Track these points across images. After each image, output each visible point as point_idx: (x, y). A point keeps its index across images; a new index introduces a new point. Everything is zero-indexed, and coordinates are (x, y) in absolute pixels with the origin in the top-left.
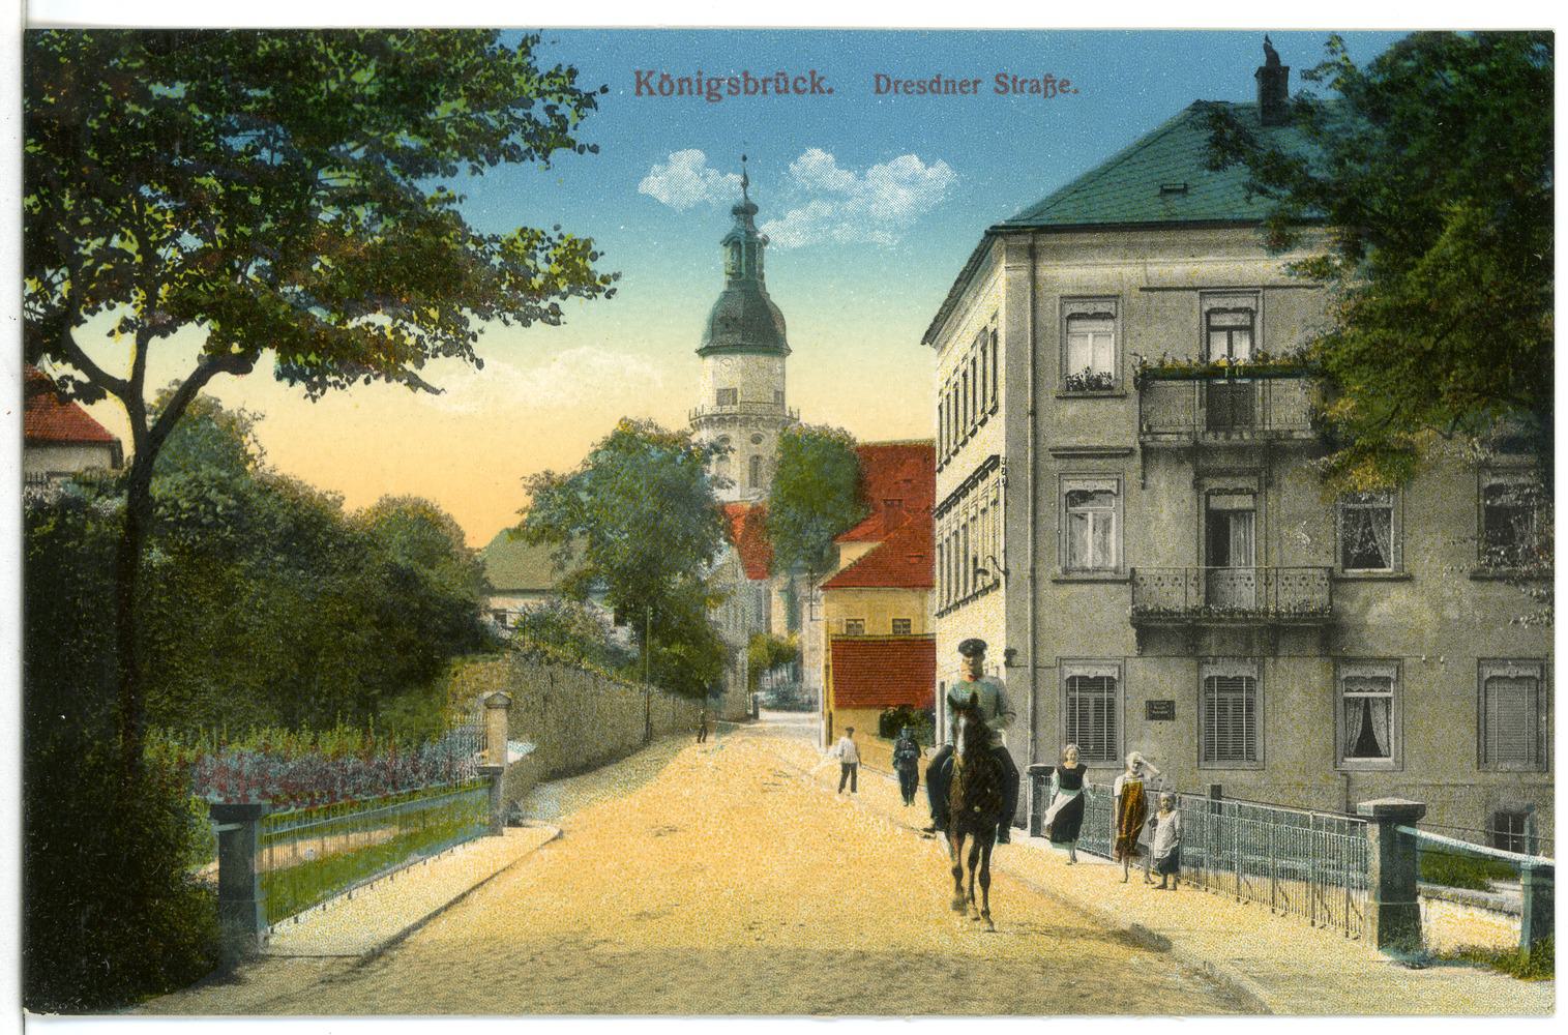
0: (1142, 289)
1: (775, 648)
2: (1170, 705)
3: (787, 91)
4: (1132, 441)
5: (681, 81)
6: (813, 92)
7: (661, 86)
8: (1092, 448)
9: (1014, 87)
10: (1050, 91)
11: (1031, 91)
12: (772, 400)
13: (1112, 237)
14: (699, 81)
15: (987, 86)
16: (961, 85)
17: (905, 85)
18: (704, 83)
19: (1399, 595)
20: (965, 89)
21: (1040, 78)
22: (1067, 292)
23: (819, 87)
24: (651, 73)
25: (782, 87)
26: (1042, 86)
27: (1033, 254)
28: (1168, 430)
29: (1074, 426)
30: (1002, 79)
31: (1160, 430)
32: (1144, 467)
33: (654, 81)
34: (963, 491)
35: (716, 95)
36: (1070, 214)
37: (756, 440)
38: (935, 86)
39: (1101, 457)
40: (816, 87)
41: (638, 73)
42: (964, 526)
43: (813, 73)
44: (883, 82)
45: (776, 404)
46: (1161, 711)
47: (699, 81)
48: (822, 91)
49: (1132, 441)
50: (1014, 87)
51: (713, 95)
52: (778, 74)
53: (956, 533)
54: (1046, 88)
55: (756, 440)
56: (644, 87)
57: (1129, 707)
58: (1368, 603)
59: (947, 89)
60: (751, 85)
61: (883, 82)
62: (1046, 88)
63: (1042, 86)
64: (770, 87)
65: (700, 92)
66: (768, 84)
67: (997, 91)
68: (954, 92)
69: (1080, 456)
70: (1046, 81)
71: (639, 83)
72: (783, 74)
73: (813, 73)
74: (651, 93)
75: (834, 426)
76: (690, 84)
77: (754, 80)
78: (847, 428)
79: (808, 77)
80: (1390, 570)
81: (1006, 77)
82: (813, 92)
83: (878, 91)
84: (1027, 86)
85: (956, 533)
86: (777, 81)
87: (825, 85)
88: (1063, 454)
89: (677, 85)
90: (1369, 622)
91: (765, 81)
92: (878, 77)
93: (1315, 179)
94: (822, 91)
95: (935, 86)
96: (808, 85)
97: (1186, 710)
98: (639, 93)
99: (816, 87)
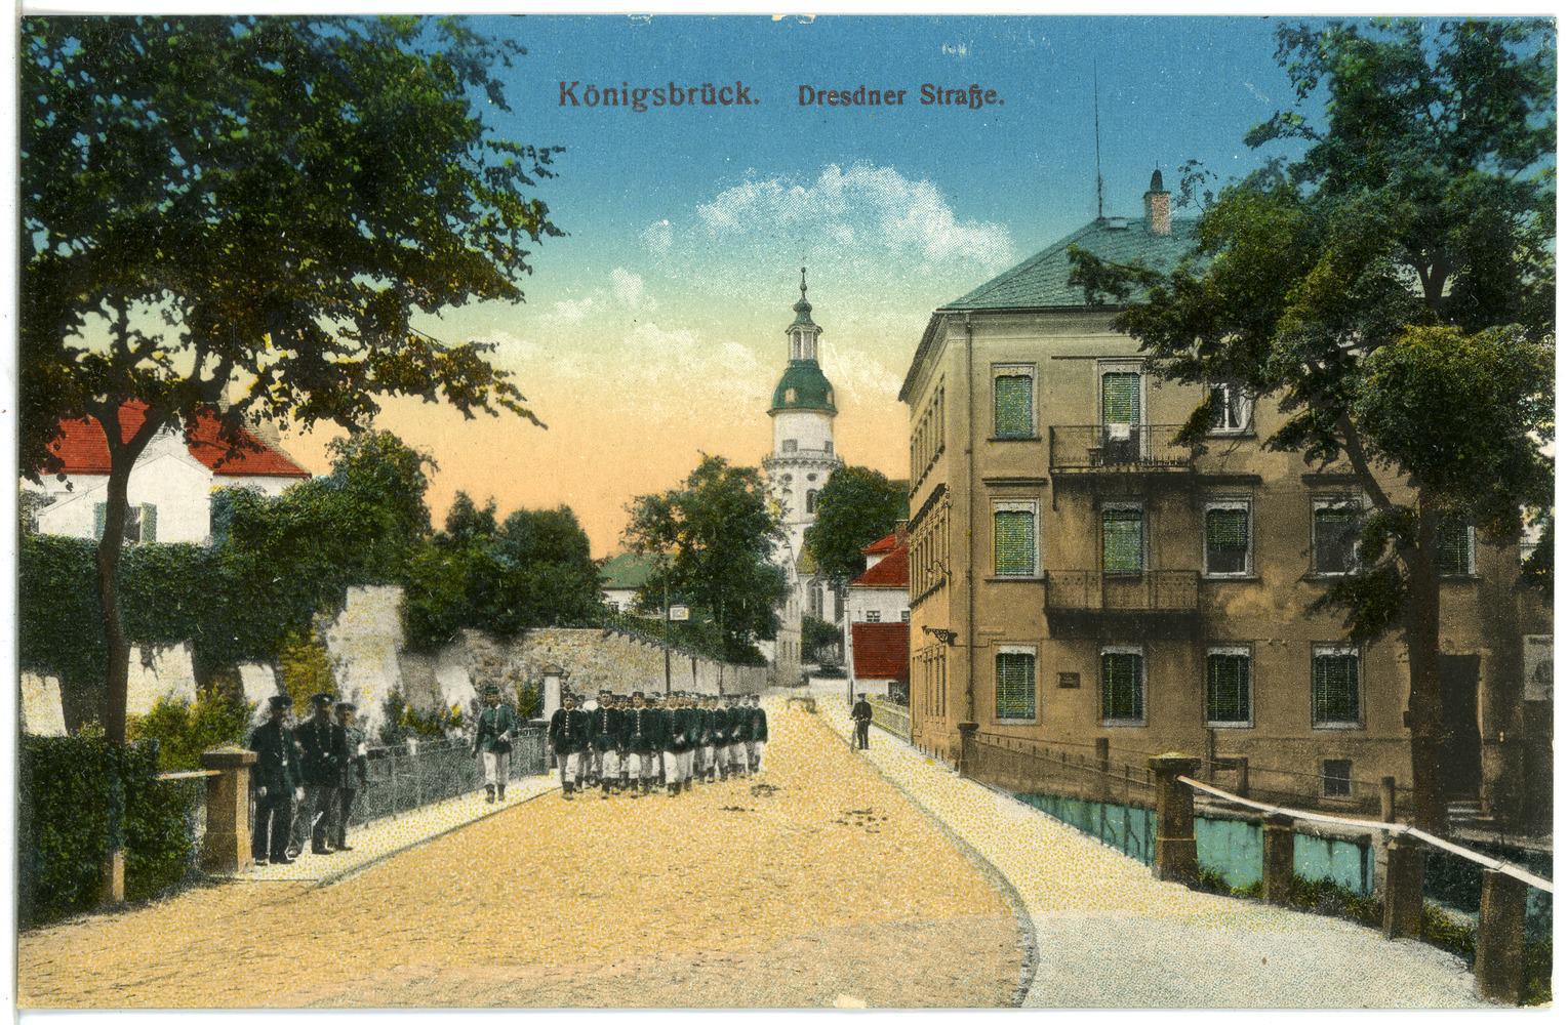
0: (1053, 358)
1: (1544, 62)
2: (1076, 676)
3: (713, 102)
4: (1044, 473)
5: (606, 92)
6: (739, 102)
7: (586, 95)
8: (1031, 479)
9: (940, 98)
10: (976, 103)
11: (958, 102)
12: (823, 448)
13: (1027, 319)
14: (625, 92)
15: (914, 94)
16: (887, 96)
17: (830, 96)
18: (630, 94)
19: (1251, 594)
20: (890, 100)
21: (967, 89)
22: (996, 359)
23: (746, 98)
24: (575, 84)
25: (708, 98)
26: (968, 96)
27: (970, 331)
28: (1073, 464)
29: (1000, 462)
30: (928, 89)
31: (1067, 464)
32: (1055, 494)
33: (579, 93)
34: (924, 512)
35: (642, 105)
36: (998, 300)
37: (812, 477)
38: (859, 97)
39: (1023, 485)
40: (742, 96)
41: (563, 85)
42: (931, 533)
43: (739, 84)
44: (807, 94)
45: (826, 452)
46: (1068, 681)
47: (625, 92)
48: (748, 102)
49: (1044, 473)
50: (940, 98)
51: (638, 104)
52: (705, 85)
53: (921, 544)
54: (972, 99)
55: (812, 477)
56: (567, 98)
57: (1044, 680)
58: (1228, 598)
59: (871, 99)
60: (677, 95)
61: (807, 94)
62: (972, 99)
63: (968, 96)
64: (698, 95)
65: (625, 102)
66: (695, 94)
67: (924, 102)
68: (878, 102)
69: (1007, 485)
70: (971, 91)
71: (563, 95)
72: (710, 85)
73: (739, 84)
74: (575, 102)
75: (871, 468)
76: (615, 94)
77: (679, 90)
78: (880, 471)
79: (735, 89)
80: (1243, 573)
81: (932, 88)
82: (739, 102)
83: (802, 102)
84: (953, 97)
85: (921, 544)
86: (704, 91)
87: (751, 96)
88: (992, 483)
89: (602, 96)
90: (1229, 612)
91: (691, 92)
92: (802, 89)
93: (1120, 326)
94: (748, 102)
95: (859, 97)
96: (735, 96)
97: (1089, 686)
98: (563, 102)
99: (742, 96)
